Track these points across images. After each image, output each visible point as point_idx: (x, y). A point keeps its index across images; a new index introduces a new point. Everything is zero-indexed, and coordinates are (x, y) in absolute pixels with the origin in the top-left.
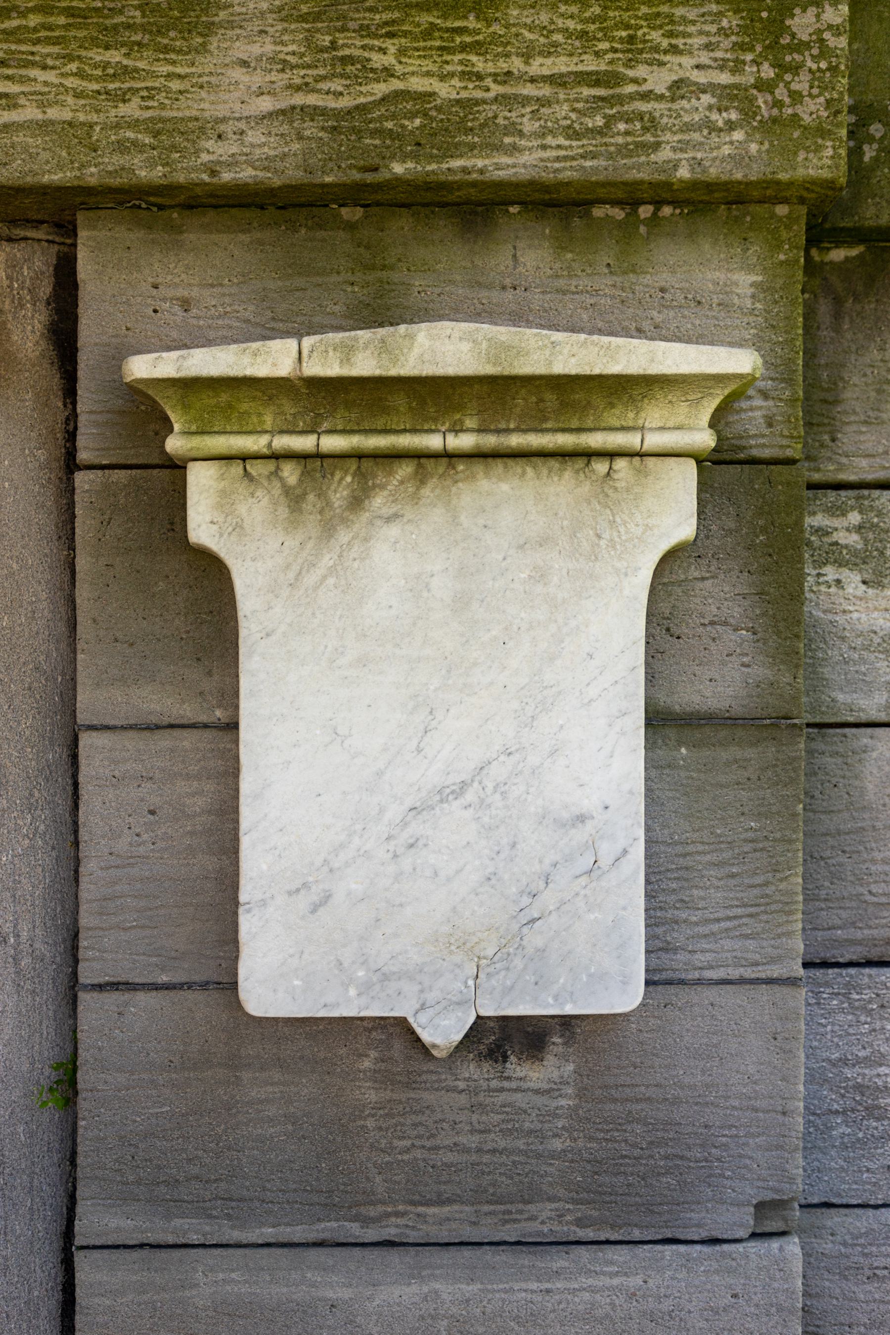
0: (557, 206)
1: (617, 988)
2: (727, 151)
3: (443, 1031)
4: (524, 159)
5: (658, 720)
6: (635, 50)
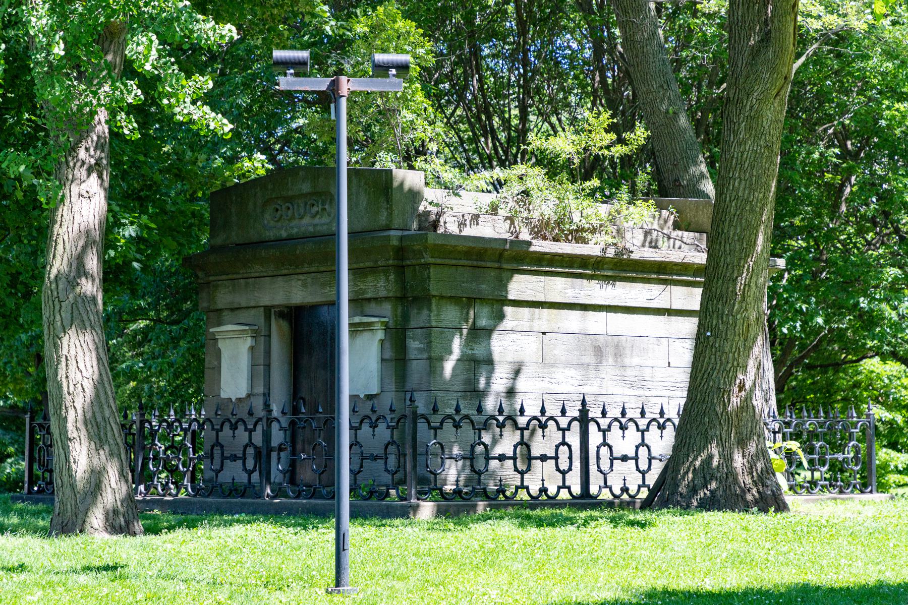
0: (375, 299)
1: (375, 390)
2: (383, 293)
3: (362, 396)
4: (368, 296)
5: (382, 360)
6: (378, 282)
